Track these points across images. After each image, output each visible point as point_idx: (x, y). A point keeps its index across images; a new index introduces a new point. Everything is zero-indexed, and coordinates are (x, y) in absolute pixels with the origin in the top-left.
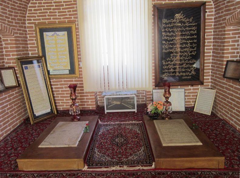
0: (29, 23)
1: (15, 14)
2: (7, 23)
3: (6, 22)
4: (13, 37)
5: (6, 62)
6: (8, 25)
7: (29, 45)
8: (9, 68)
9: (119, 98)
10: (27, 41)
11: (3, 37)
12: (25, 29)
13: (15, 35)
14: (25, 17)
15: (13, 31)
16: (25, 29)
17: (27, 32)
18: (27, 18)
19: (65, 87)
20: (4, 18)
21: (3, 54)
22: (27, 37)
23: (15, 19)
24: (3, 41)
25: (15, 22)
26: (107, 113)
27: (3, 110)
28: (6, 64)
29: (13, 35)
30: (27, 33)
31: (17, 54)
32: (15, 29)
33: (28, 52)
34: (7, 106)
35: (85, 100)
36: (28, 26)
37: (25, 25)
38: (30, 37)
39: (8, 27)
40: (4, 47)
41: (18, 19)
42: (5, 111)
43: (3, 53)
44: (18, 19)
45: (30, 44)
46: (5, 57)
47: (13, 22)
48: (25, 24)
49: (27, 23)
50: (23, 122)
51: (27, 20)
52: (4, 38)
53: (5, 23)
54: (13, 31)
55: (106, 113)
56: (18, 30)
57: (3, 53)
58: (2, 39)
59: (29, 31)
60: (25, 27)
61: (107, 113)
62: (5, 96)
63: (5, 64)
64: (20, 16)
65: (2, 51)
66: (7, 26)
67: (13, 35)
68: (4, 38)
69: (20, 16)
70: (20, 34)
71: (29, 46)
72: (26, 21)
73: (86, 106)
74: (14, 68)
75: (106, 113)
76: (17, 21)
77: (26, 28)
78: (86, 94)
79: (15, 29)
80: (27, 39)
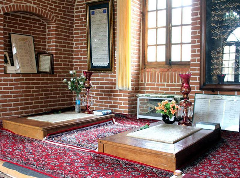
0: (76, 12)
1: (60, 2)
2: (48, 10)
3: (48, 9)
4: (55, 23)
5: (47, 49)
6: (49, 11)
7: (74, 34)
8: (49, 54)
9: (110, 66)
10: (72, 30)
11: (48, 25)
12: (72, 18)
13: (57, 22)
14: (74, 6)
15: (55, 18)
16: (72, 18)
17: (74, 21)
18: (75, 7)
19: (13, 30)
20: (46, 4)
21: (46, 41)
22: (73, 27)
23: (59, 7)
24: (47, 29)
25: (59, 9)
26: (139, 118)
27: (28, 90)
28: (47, 51)
29: (55, 21)
30: (74, 23)
31: (55, 41)
32: (58, 17)
33: (72, 42)
34: (33, 88)
35: (118, 101)
36: (76, 15)
37: (73, 14)
38: (76, 26)
39: (49, 13)
40: (48, 34)
41: (63, 7)
42: (30, 91)
43: (46, 40)
44: (63, 7)
45: (76, 34)
46: (46, 44)
47: (57, 9)
48: (73, 12)
49: (74, 12)
50: (49, 111)
51: (76, 9)
52: (48, 26)
53: (47, 9)
54: (55, 18)
55: (138, 119)
56: (62, 17)
57: (46, 40)
58: (47, 26)
59: (76, 20)
60: (73, 16)
61: (139, 118)
62: (67, 98)
63: (46, 50)
64: (66, 4)
65: (45, 38)
66: (48, 12)
67: (55, 21)
68: (48, 26)
69: (66, 4)
70: (64, 22)
71: (74, 36)
72: (74, 10)
73: (118, 109)
74: (52, 55)
75: (138, 119)
76: (62, 9)
77: (73, 17)
78: (52, 52)
79: (58, 17)
80: (73, 29)
